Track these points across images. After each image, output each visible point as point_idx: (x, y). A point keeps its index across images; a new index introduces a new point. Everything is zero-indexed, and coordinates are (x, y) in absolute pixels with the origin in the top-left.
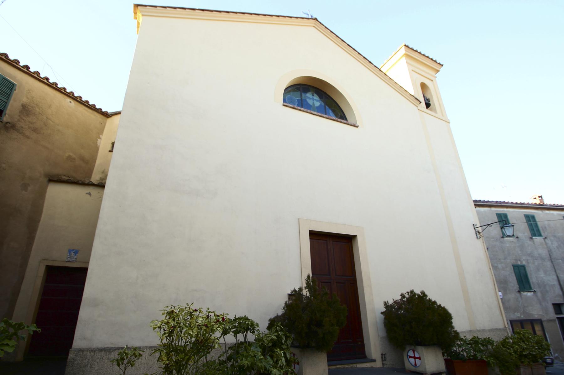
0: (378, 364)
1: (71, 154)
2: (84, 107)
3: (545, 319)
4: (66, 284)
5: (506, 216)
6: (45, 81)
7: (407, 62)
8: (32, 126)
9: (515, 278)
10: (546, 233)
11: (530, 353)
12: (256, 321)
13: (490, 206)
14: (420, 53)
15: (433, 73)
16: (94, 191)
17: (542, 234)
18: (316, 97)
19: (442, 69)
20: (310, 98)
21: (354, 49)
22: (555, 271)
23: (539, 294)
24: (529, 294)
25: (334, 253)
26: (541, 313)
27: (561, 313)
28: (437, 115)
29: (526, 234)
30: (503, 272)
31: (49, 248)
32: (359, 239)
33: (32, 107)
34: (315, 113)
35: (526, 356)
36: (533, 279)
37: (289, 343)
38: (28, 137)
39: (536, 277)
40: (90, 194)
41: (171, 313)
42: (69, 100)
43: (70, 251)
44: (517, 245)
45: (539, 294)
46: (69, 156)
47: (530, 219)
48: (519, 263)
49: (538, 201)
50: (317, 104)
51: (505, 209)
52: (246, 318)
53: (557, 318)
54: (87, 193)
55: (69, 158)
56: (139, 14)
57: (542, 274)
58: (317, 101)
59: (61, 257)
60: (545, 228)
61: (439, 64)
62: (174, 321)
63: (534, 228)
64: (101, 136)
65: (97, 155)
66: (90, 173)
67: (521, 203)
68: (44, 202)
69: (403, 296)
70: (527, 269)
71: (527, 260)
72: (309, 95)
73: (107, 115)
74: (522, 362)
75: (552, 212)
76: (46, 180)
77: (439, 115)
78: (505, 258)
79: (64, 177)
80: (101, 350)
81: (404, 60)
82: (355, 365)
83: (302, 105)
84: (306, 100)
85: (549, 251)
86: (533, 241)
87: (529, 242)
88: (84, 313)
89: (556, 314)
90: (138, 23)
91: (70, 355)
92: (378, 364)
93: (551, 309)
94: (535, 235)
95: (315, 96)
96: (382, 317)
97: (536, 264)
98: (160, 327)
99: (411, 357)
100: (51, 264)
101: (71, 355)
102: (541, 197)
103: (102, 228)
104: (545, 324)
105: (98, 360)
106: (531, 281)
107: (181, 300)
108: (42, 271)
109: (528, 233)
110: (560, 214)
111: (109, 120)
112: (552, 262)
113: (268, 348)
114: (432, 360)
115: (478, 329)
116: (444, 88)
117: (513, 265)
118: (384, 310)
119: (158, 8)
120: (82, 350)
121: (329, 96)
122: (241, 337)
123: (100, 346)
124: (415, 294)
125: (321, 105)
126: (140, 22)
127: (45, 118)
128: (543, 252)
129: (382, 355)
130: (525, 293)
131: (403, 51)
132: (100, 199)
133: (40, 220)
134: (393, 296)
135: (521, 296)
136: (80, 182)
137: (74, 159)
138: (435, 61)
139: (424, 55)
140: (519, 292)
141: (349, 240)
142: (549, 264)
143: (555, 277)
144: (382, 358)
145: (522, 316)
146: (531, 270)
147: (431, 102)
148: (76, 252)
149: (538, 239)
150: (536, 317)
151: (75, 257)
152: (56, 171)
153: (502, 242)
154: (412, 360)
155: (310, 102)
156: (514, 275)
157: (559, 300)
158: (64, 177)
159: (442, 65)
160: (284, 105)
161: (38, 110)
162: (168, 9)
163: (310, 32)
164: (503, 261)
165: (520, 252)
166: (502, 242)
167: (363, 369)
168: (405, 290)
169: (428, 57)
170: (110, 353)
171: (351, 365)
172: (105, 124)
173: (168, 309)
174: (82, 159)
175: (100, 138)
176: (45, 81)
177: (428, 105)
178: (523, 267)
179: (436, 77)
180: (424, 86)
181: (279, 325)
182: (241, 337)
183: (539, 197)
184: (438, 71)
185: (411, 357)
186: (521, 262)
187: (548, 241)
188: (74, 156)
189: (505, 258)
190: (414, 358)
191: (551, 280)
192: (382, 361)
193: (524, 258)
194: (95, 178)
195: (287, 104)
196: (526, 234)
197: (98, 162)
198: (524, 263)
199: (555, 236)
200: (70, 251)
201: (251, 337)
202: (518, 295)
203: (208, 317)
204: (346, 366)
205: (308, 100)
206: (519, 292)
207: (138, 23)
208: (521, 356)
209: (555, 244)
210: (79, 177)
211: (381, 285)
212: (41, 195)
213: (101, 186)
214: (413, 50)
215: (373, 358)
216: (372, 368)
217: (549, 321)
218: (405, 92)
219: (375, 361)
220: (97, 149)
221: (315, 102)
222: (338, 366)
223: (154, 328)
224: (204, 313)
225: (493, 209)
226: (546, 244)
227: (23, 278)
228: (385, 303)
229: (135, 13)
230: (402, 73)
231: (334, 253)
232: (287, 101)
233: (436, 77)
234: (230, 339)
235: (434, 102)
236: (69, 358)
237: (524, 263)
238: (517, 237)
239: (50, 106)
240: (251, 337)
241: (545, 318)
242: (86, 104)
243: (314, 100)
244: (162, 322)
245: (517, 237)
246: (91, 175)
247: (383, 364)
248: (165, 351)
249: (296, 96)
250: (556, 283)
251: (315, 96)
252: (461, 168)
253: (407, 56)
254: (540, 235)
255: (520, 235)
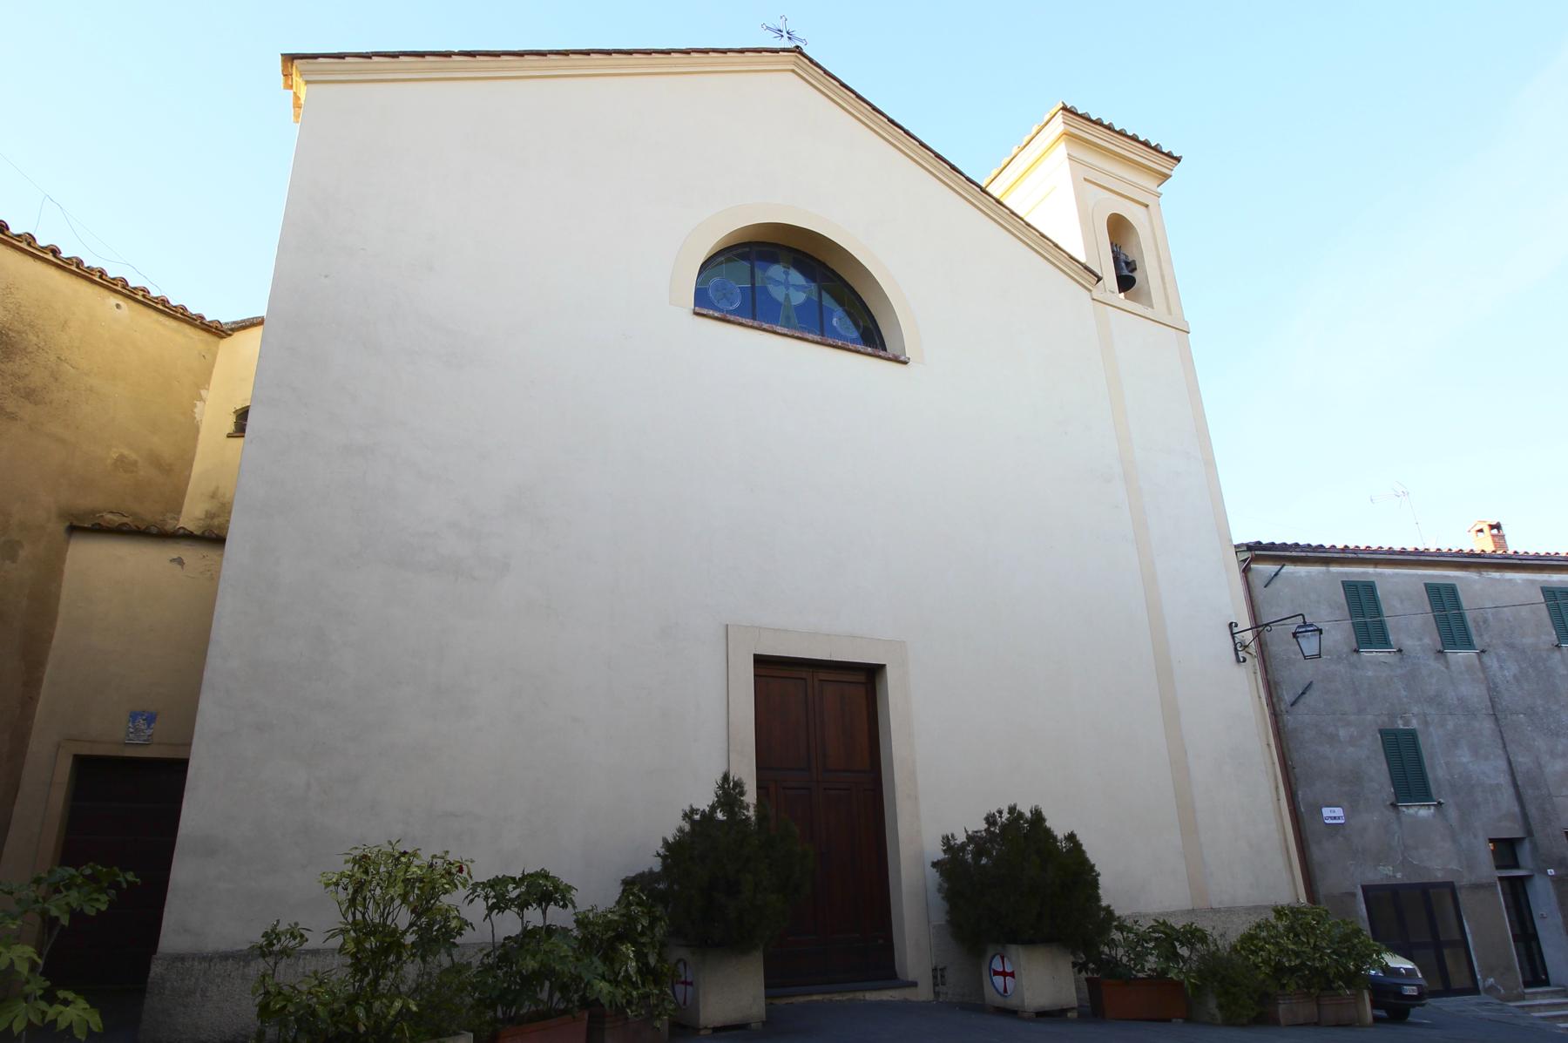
0: (924, 993)
1: (126, 452)
2: (155, 315)
3: (1465, 882)
4: (131, 801)
5: (1370, 588)
6: (50, 257)
7: (1070, 157)
8: (20, 384)
9: (1385, 766)
10: (1486, 638)
11: (1303, 964)
12: (565, 879)
13: (1327, 561)
14: (1110, 128)
15: (1149, 183)
16: (192, 555)
17: (1476, 640)
18: (796, 277)
19: (1178, 171)
20: (777, 283)
21: (907, 132)
22: (1505, 746)
23: (1453, 814)
24: (1423, 812)
25: (821, 715)
26: (1454, 866)
27: (1516, 866)
28: (1148, 312)
29: (1427, 641)
30: (1351, 749)
31: (79, 709)
32: (891, 675)
33: (19, 332)
34: (785, 331)
35: (1292, 970)
36: (1437, 770)
37: (660, 930)
38: (12, 417)
39: (1447, 764)
40: (180, 561)
41: (363, 861)
42: (114, 300)
43: (134, 716)
44: (1399, 671)
45: (1453, 814)
46: (122, 458)
47: (1443, 600)
48: (1400, 725)
49: (1485, 544)
50: (798, 298)
51: (1371, 570)
52: (545, 875)
53: (1501, 879)
54: (173, 560)
55: (121, 462)
56: (297, 79)
57: (1464, 756)
58: (798, 288)
59: (110, 734)
60: (1485, 621)
61: (1169, 155)
62: (363, 877)
63: (1450, 619)
64: (203, 392)
65: (195, 447)
66: (175, 503)
67: (1416, 552)
68: (60, 586)
69: (991, 820)
70: (1421, 739)
71: (1425, 715)
72: (776, 271)
73: (218, 331)
74: (1283, 986)
75: (1509, 575)
76: (62, 527)
77: (1159, 311)
78: (1360, 711)
79: (109, 516)
80: (225, 957)
81: (1062, 150)
82: (859, 995)
83: (755, 311)
84: (765, 290)
85: (1489, 689)
86: (1447, 662)
87: (1435, 664)
88: (182, 871)
89: (1498, 867)
90: (297, 97)
91: (153, 967)
92: (924, 993)
93: (1485, 852)
94: (1454, 645)
95: (792, 280)
96: (933, 876)
97: (1450, 725)
98: (337, 884)
99: (997, 973)
100: (85, 750)
101: (156, 969)
102: (1498, 527)
103: (222, 661)
104: (1463, 897)
105: (218, 980)
106: (1430, 776)
107: (376, 836)
108: (65, 767)
109: (1432, 639)
110: (1533, 582)
111: (225, 344)
112: (1497, 719)
113: (602, 938)
114: (1040, 979)
115: (1215, 906)
116: (1177, 228)
117: (1381, 732)
118: (662, 851)
119: (348, 59)
120: (181, 958)
121: (833, 271)
122: (534, 916)
123: (224, 947)
124: (1021, 815)
125: (808, 299)
126: (303, 97)
127: (53, 358)
128: (1474, 692)
129: (935, 970)
130: (1412, 811)
131: (1058, 125)
132: (214, 578)
133: (51, 637)
134: (967, 821)
135: (1399, 819)
136: (154, 530)
137: (135, 463)
138: (1157, 149)
139: (1122, 133)
140: (1394, 805)
141: (871, 674)
142: (1487, 726)
143: (1503, 764)
144: (935, 977)
145: (1399, 875)
146: (1433, 744)
147: (1137, 275)
148: (151, 719)
149: (1460, 656)
150: (1439, 876)
151: (149, 732)
152: (86, 502)
153: (1353, 666)
154: (999, 980)
155: (778, 293)
156: (1382, 758)
157: (1512, 830)
158: (109, 516)
159: (1178, 159)
160: (696, 314)
161: (35, 340)
162: (375, 59)
163: (785, 88)
164: (1352, 718)
165: (1403, 693)
166: (1353, 666)
167: (881, 1004)
168: (1000, 803)
169: (1134, 138)
170: (247, 964)
171: (851, 996)
172: (214, 357)
173: (358, 853)
174: (156, 461)
175: (201, 399)
176: (50, 257)
177: (1126, 282)
178: (1412, 736)
179: (1159, 195)
180: (1118, 227)
181: (635, 890)
182: (534, 916)
183: (1492, 527)
184: (1167, 177)
185: (997, 973)
186: (1407, 722)
187: (1491, 661)
188: (134, 456)
189: (1360, 711)
190: (1004, 974)
191: (1491, 771)
192: (935, 985)
193: (1415, 710)
194: (191, 515)
195: (705, 311)
196: (1427, 641)
197: (197, 468)
198: (1414, 724)
199: (1512, 646)
200: (134, 716)
201: (559, 916)
202: (1391, 814)
203: (431, 866)
204: (837, 997)
205: (771, 287)
206: (1394, 805)
207: (297, 97)
208: (1279, 970)
209: (1512, 669)
210: (149, 512)
211: (938, 794)
212: (52, 569)
213: (214, 538)
214: (1089, 120)
215: (911, 978)
216: (906, 1001)
217: (1476, 887)
218: (1054, 251)
219: (914, 984)
220: (193, 430)
221: (792, 291)
222: (815, 998)
223: (327, 885)
224: (425, 858)
225: (1334, 569)
226: (1484, 668)
227: (16, 787)
228: (947, 840)
229: (287, 74)
230: (1055, 196)
231: (821, 715)
232: (705, 302)
233: (1159, 195)
234: (509, 924)
235: (1149, 271)
236: (152, 974)
237: (1414, 724)
238: (1400, 651)
239: (64, 325)
240: (559, 916)
241: (1466, 879)
242: (162, 307)
243: (788, 285)
244: (342, 875)
245: (1400, 651)
246: (181, 505)
247: (937, 994)
248: (352, 934)
249: (737, 277)
250: (1504, 779)
251: (792, 280)
252: (1210, 463)
253: (1070, 136)
254: (1469, 644)
255: (1408, 643)
